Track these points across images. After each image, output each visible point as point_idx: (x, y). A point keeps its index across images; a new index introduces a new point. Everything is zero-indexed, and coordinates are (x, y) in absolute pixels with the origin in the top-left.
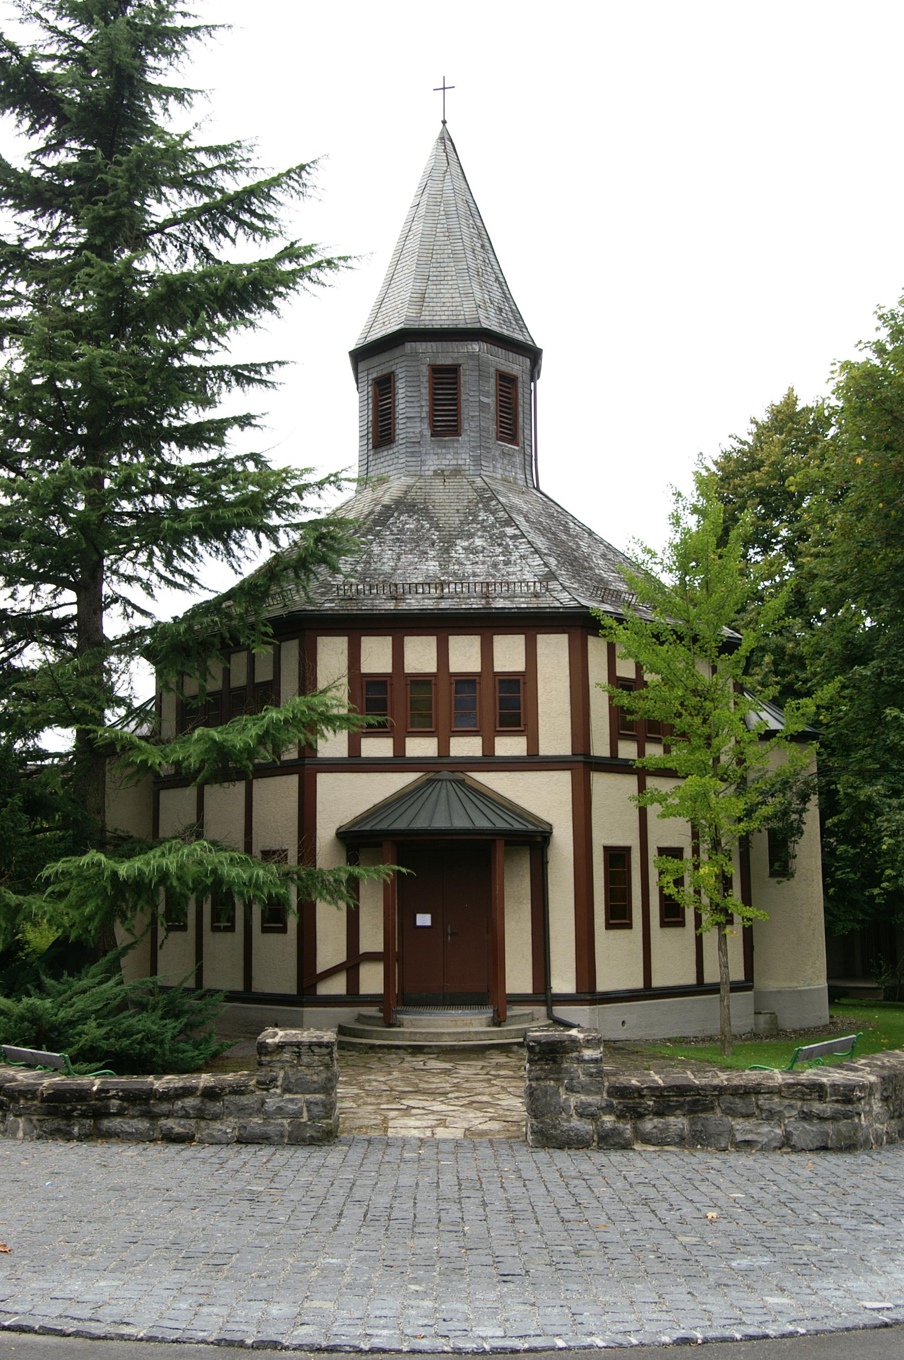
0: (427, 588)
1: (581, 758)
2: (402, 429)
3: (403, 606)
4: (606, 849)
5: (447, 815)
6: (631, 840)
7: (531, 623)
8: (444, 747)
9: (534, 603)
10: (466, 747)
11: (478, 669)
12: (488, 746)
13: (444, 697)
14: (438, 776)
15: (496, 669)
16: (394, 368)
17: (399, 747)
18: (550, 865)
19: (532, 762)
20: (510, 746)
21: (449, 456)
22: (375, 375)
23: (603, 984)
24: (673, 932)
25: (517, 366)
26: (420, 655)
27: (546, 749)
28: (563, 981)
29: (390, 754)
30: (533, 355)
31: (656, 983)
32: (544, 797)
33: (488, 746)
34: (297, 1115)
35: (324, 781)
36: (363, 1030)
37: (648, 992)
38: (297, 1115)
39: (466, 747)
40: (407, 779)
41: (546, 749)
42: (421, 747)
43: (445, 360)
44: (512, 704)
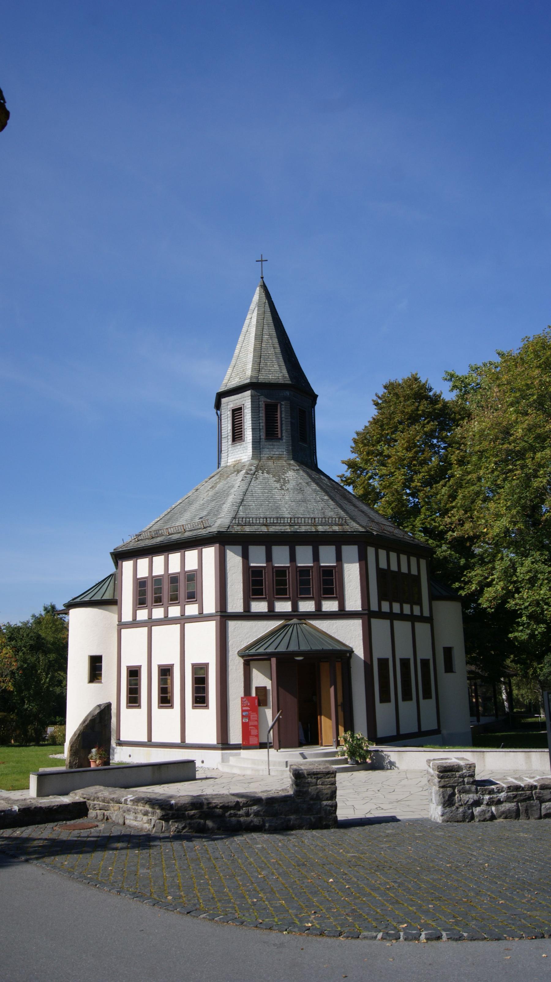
1: (366, 612)
2: (248, 434)
3: (347, 528)
4: (193, 665)
6: (410, 656)
7: (338, 540)
8: (295, 607)
9: (264, 529)
10: (306, 606)
12: (319, 606)
13: (290, 579)
17: (271, 607)
18: (352, 669)
19: (342, 614)
20: (330, 606)
21: (275, 450)
26: (281, 557)
27: (206, 611)
29: (266, 610)
31: (154, 740)
32: (349, 634)
33: (319, 606)
35: (232, 625)
36: (317, 757)
37: (149, 744)
39: (306, 606)
41: (206, 611)
42: (283, 607)
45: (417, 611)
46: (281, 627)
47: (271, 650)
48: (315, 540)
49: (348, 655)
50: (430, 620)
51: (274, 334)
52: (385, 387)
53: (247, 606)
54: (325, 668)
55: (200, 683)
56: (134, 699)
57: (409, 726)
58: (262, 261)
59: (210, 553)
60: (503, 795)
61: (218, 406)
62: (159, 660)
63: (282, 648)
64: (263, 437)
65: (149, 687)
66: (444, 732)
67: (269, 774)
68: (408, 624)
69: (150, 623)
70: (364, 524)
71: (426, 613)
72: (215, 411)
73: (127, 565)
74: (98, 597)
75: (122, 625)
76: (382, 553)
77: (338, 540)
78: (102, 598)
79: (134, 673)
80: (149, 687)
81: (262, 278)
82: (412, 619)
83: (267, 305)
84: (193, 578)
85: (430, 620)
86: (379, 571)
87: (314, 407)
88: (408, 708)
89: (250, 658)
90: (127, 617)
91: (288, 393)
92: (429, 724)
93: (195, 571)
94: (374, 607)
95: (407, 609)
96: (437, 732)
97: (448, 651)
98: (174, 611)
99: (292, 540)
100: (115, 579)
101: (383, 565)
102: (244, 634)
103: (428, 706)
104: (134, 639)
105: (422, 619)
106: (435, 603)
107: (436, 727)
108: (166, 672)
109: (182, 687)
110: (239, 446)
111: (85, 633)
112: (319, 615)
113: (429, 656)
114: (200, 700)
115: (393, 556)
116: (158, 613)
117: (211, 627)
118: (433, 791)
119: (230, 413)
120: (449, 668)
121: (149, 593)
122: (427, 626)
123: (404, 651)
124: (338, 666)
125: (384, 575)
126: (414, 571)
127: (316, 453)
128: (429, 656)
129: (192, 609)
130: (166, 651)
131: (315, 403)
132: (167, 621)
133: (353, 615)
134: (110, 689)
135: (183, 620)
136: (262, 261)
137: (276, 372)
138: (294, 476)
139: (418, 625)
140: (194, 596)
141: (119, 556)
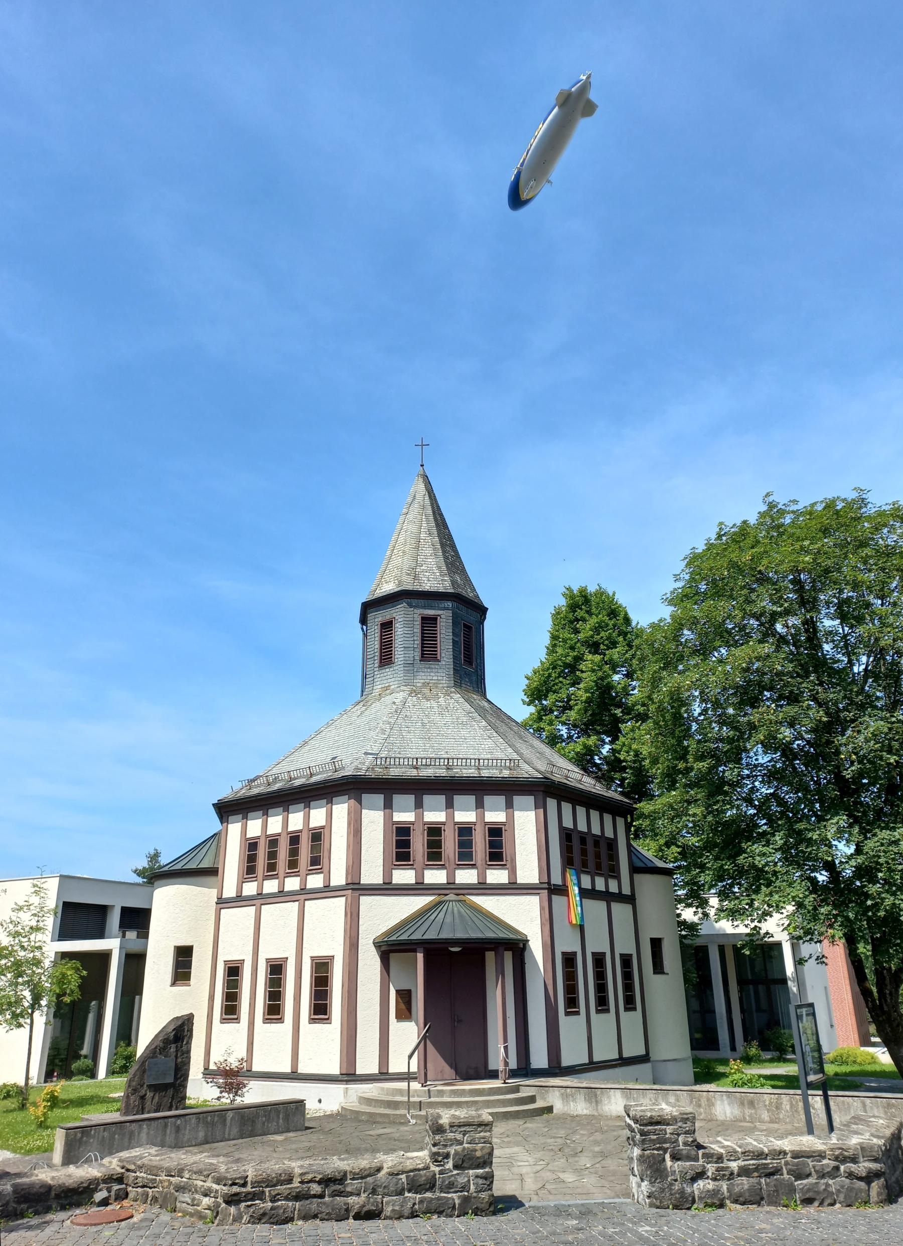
0: (459, 764)
2: (399, 654)
4: (563, 954)
5: (449, 927)
6: (577, 948)
7: (509, 789)
8: (451, 876)
9: (414, 773)
10: (467, 876)
14: (447, 898)
16: (394, 615)
19: (513, 888)
23: (566, 1062)
25: (473, 617)
30: (482, 611)
32: (523, 916)
35: (366, 901)
39: (467, 876)
40: (419, 902)
42: (436, 876)
45: (613, 887)
47: (417, 936)
48: (480, 788)
49: (521, 945)
50: (630, 899)
52: (671, 602)
53: (388, 874)
54: (490, 956)
55: (321, 983)
56: (231, 1010)
57: (605, 1051)
59: (341, 810)
61: (363, 621)
62: (269, 951)
63: (431, 935)
64: (418, 658)
65: (253, 991)
66: (654, 1056)
68: (603, 905)
69: (261, 898)
70: (543, 769)
71: (626, 891)
74: (193, 865)
75: (222, 903)
77: (509, 789)
78: (197, 870)
79: (234, 971)
80: (253, 991)
81: (422, 466)
82: (607, 897)
83: (427, 498)
85: (630, 899)
86: (562, 830)
87: (482, 623)
88: (603, 1024)
89: (391, 949)
90: (230, 892)
91: (450, 604)
93: (323, 827)
94: (556, 880)
95: (600, 884)
96: (644, 1059)
97: (656, 944)
98: (293, 884)
99: (450, 787)
100: (217, 840)
101: (568, 823)
102: (384, 915)
103: (632, 1020)
104: (238, 920)
105: (620, 898)
106: (637, 877)
108: (276, 969)
109: (298, 990)
110: (388, 671)
111: (175, 912)
112: (483, 888)
114: (320, 1010)
116: (271, 886)
117: (339, 904)
119: (377, 629)
120: (658, 968)
121: (258, 859)
122: (628, 908)
123: (597, 943)
124: (508, 957)
125: (567, 836)
126: (609, 833)
129: (315, 881)
130: (278, 943)
131: (485, 618)
132: (282, 896)
133: (527, 889)
134: (198, 998)
135: (305, 894)
136: (422, 445)
137: (433, 578)
139: (615, 906)
140: (317, 862)
141: (227, 810)
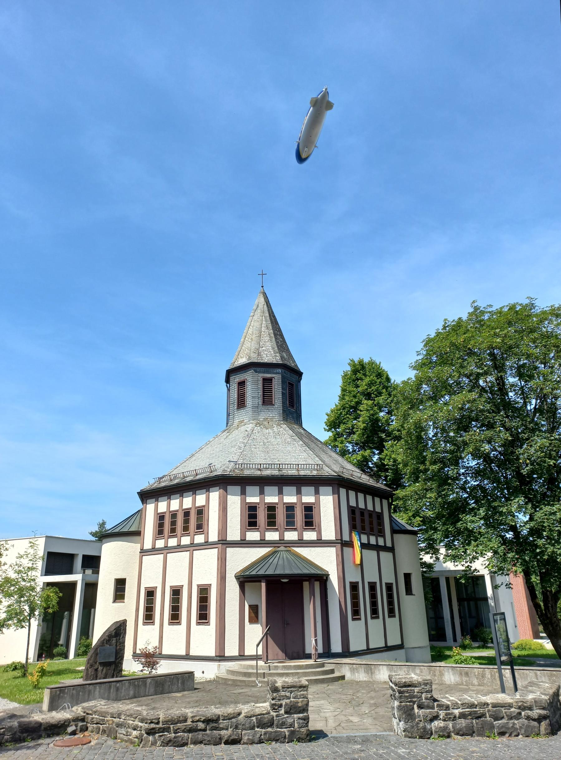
1: (339, 541)
2: (249, 401)
4: (351, 583)
5: (281, 567)
6: (359, 579)
7: (317, 482)
9: (258, 473)
10: (291, 536)
11: (314, 501)
15: (284, 502)
19: (320, 543)
20: (310, 536)
22: (238, 380)
23: (352, 648)
24: (375, 621)
25: (294, 378)
28: (336, 647)
30: (299, 374)
32: (326, 560)
34: (292, 725)
35: (230, 551)
38: (292, 725)
39: (291, 536)
40: (263, 551)
43: (268, 376)
44: (310, 518)
45: (381, 542)
46: (271, 553)
47: (261, 572)
48: (299, 482)
49: (325, 578)
50: (391, 550)
51: (270, 326)
53: (243, 534)
55: (204, 600)
56: (149, 617)
57: (377, 642)
58: (263, 274)
59: (215, 495)
60: (457, 712)
61: (227, 381)
62: (172, 582)
63: (270, 572)
65: (163, 605)
66: (406, 645)
67: (321, 105)
69: (167, 549)
70: (337, 470)
71: (389, 544)
72: (225, 384)
73: (150, 507)
74: (125, 530)
75: (144, 552)
76: (352, 494)
77: (317, 482)
79: (150, 593)
80: (163, 605)
81: (262, 287)
82: (377, 548)
84: (201, 512)
85: (391, 550)
87: (300, 382)
88: (375, 625)
89: (245, 580)
90: (148, 545)
92: (394, 640)
94: (346, 538)
95: (373, 540)
96: (400, 647)
97: (407, 576)
98: (186, 540)
100: (140, 514)
101: (353, 503)
102: (241, 559)
103: (393, 623)
104: (153, 563)
105: (385, 548)
106: (396, 536)
107: (399, 642)
108: (176, 592)
109: (189, 605)
111: (115, 559)
112: (301, 543)
113: (392, 580)
114: (203, 617)
115: (361, 496)
116: (173, 542)
117: (214, 553)
118: (396, 705)
120: (409, 591)
122: (390, 555)
123: (371, 576)
124: (317, 585)
126: (378, 509)
127: (301, 416)
128: (392, 580)
129: (199, 539)
130: (177, 576)
132: (180, 548)
137: (270, 355)
138: (284, 431)
139: (382, 554)
140: (200, 527)
141: (146, 496)
